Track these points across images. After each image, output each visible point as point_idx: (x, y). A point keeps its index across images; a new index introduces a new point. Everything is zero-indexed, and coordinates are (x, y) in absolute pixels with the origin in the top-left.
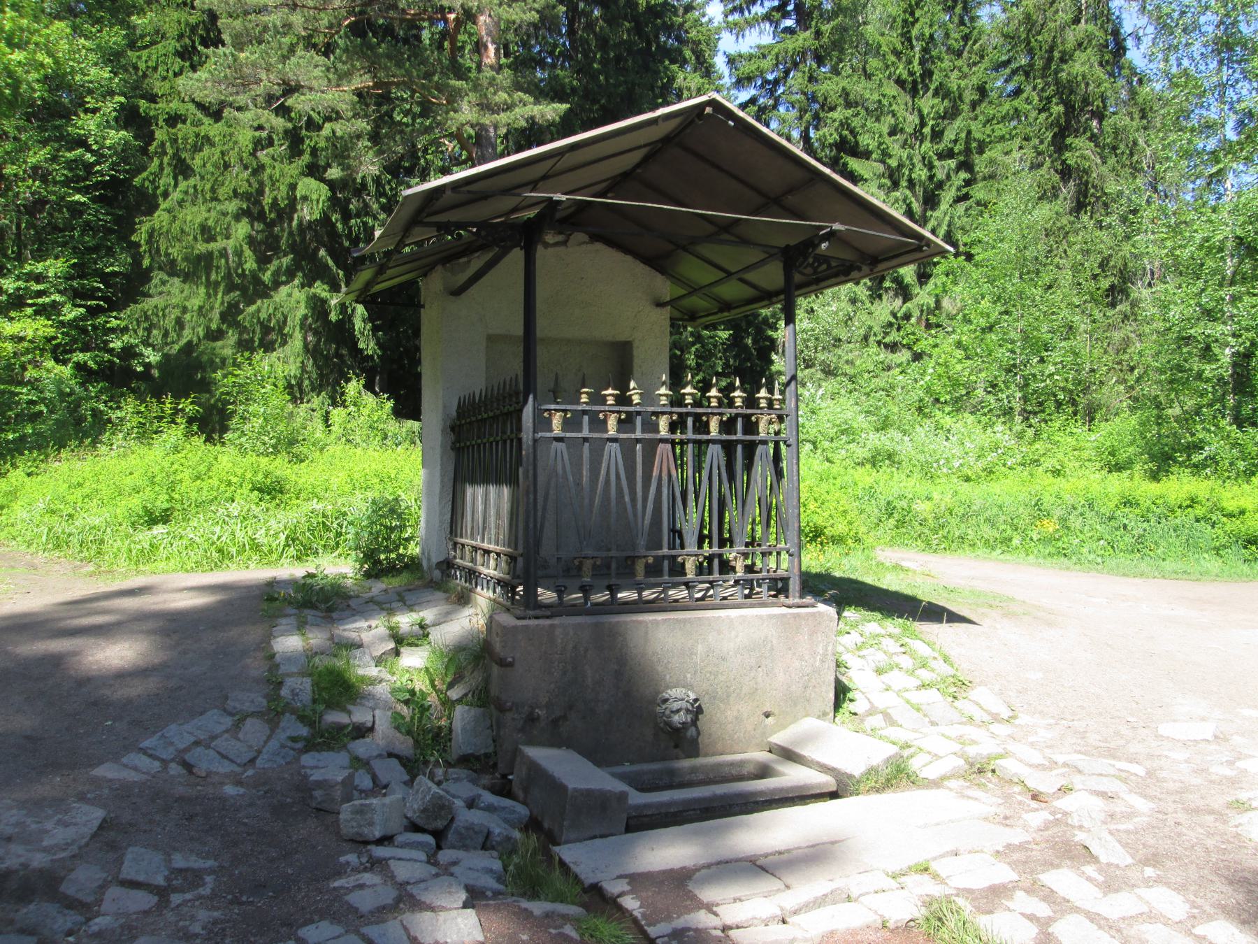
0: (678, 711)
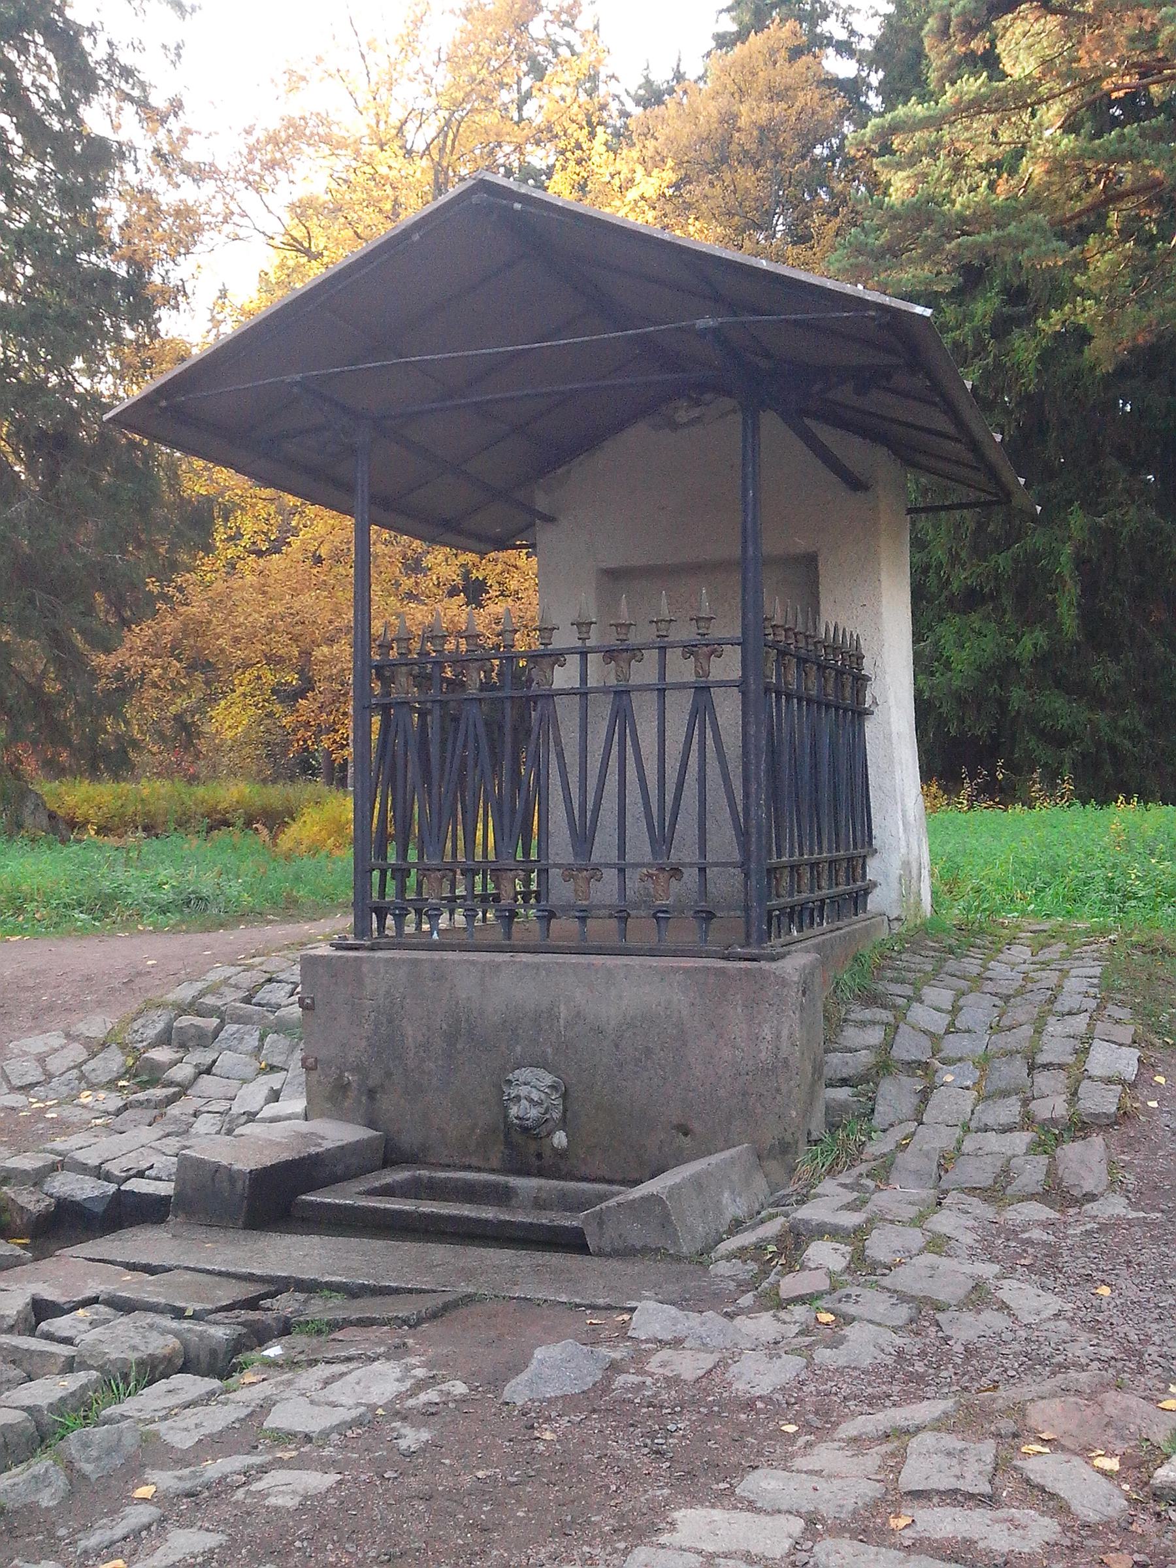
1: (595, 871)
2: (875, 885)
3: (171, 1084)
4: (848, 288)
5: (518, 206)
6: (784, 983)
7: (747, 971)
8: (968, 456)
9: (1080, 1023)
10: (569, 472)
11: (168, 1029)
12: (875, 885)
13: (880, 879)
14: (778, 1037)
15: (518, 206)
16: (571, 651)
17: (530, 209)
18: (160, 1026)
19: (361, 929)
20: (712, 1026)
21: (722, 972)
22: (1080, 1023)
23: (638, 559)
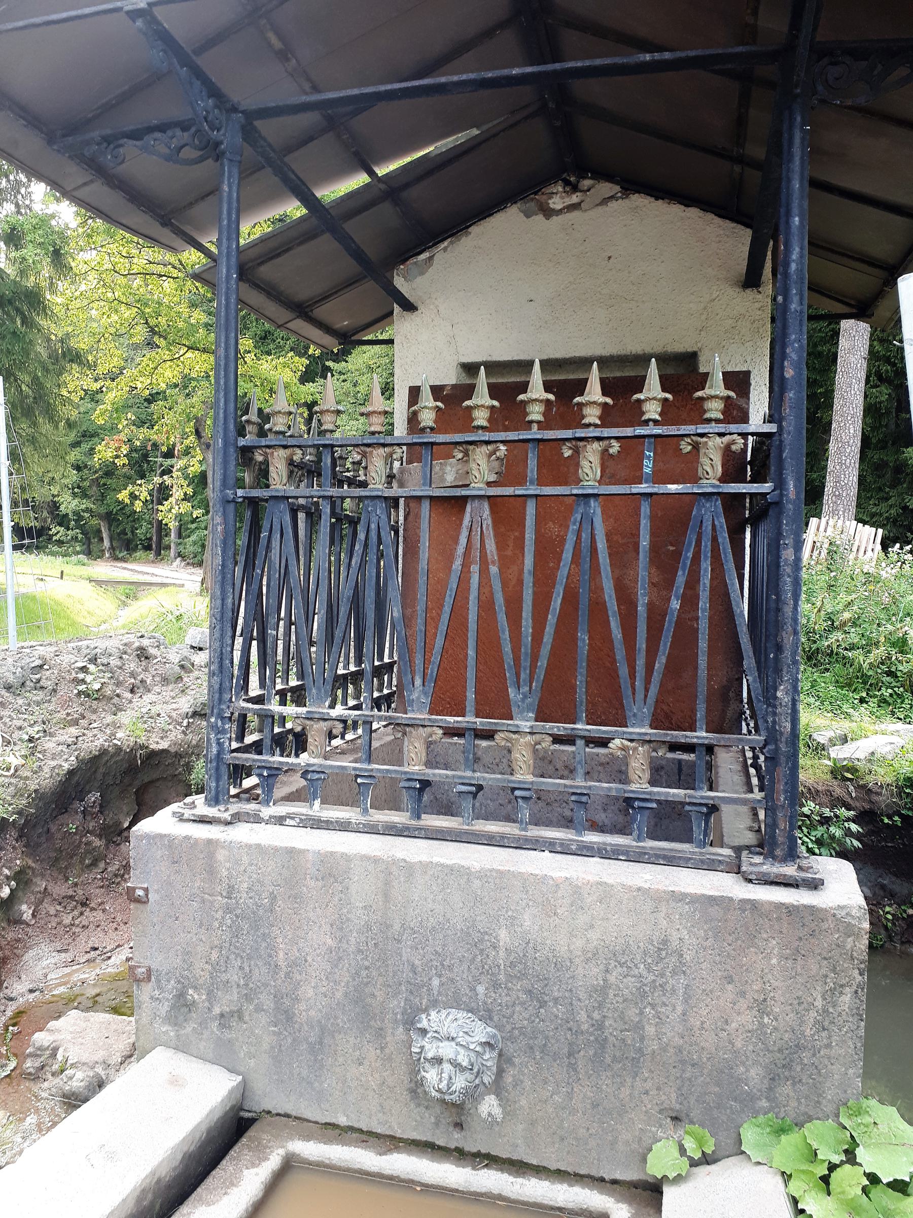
0: (438, 1061)
7: (791, 910)
10: (431, 258)
20: (730, 980)
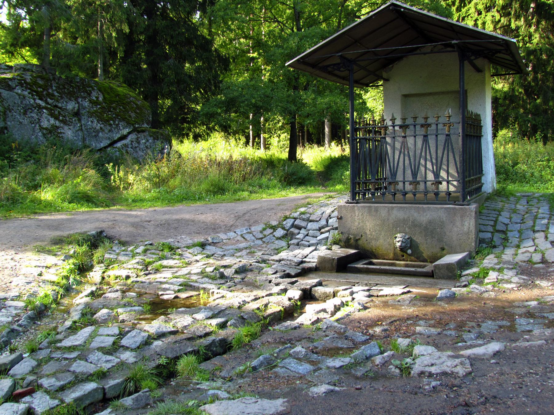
1: (418, 183)
2: (483, 184)
3: (298, 239)
4: (504, 38)
5: (402, 10)
6: (472, 211)
7: (461, 209)
8: (511, 59)
9: (545, 221)
10: (393, 67)
11: (293, 224)
12: (483, 184)
13: (485, 182)
14: (469, 224)
15: (402, 10)
16: (411, 125)
17: (406, 11)
18: (291, 223)
19: (353, 198)
21: (455, 208)
22: (545, 221)
23: (413, 92)
